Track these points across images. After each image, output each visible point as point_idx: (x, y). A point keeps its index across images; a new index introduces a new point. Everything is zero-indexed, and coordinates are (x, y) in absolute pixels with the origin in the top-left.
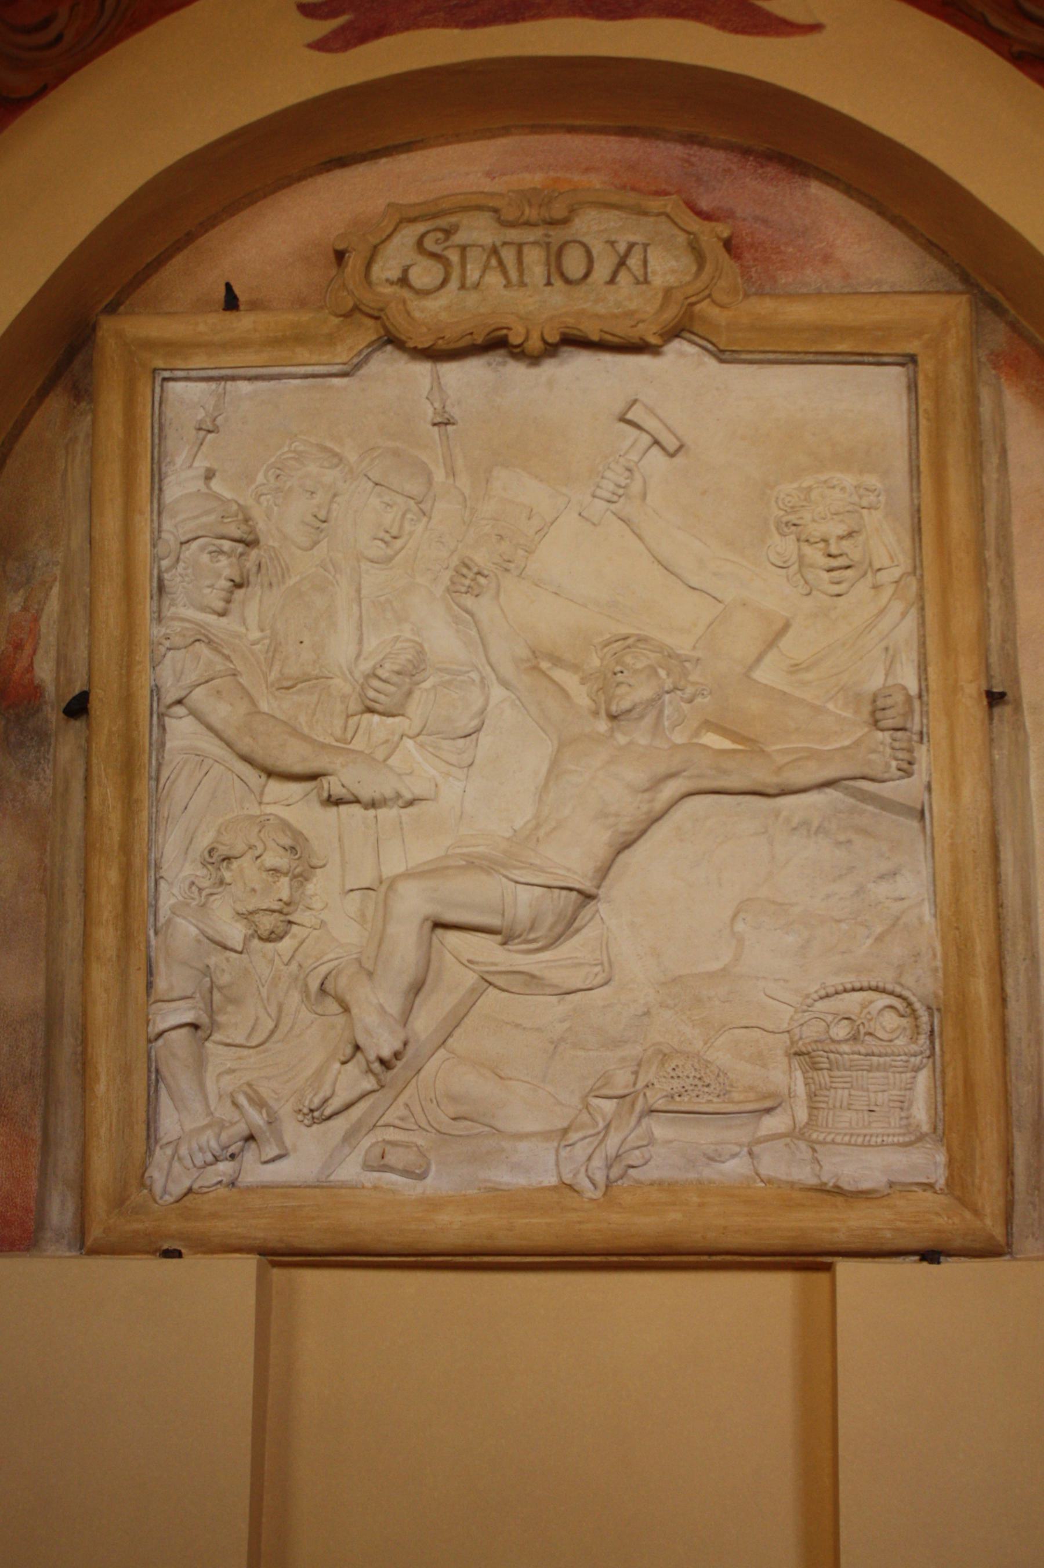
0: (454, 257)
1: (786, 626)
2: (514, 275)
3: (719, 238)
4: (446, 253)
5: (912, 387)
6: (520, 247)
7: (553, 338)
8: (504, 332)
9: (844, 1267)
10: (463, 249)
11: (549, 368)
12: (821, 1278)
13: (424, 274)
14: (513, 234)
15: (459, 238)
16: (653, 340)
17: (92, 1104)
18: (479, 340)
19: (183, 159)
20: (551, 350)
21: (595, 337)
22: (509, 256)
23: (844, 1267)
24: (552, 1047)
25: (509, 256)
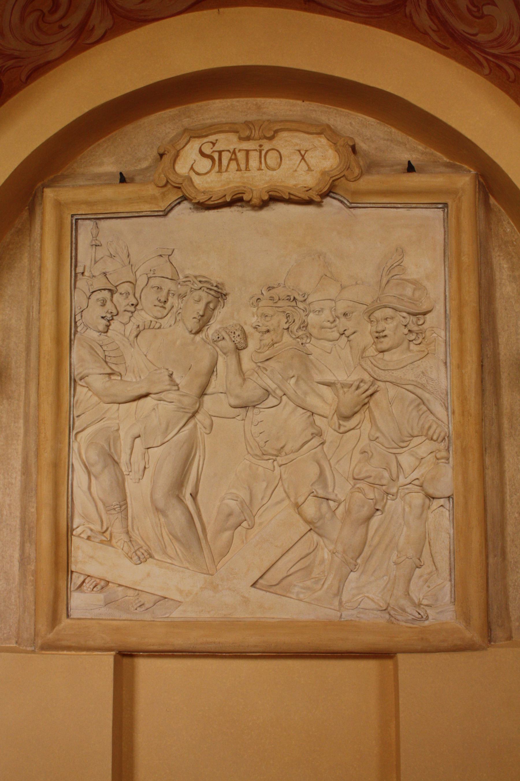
0: (216, 156)
1: (174, 250)
2: (243, 166)
3: (349, 145)
4: (213, 154)
5: (446, 219)
6: (247, 152)
7: (266, 198)
8: (241, 195)
9: (400, 656)
10: (220, 153)
11: (265, 214)
12: (389, 663)
13: (204, 165)
14: (246, 145)
15: (217, 147)
16: (317, 199)
17: (10, 367)
18: (228, 199)
19: (33, 152)
20: (264, 204)
21: (286, 197)
22: (241, 156)
23: (400, 656)
24: (104, 322)
25: (241, 156)
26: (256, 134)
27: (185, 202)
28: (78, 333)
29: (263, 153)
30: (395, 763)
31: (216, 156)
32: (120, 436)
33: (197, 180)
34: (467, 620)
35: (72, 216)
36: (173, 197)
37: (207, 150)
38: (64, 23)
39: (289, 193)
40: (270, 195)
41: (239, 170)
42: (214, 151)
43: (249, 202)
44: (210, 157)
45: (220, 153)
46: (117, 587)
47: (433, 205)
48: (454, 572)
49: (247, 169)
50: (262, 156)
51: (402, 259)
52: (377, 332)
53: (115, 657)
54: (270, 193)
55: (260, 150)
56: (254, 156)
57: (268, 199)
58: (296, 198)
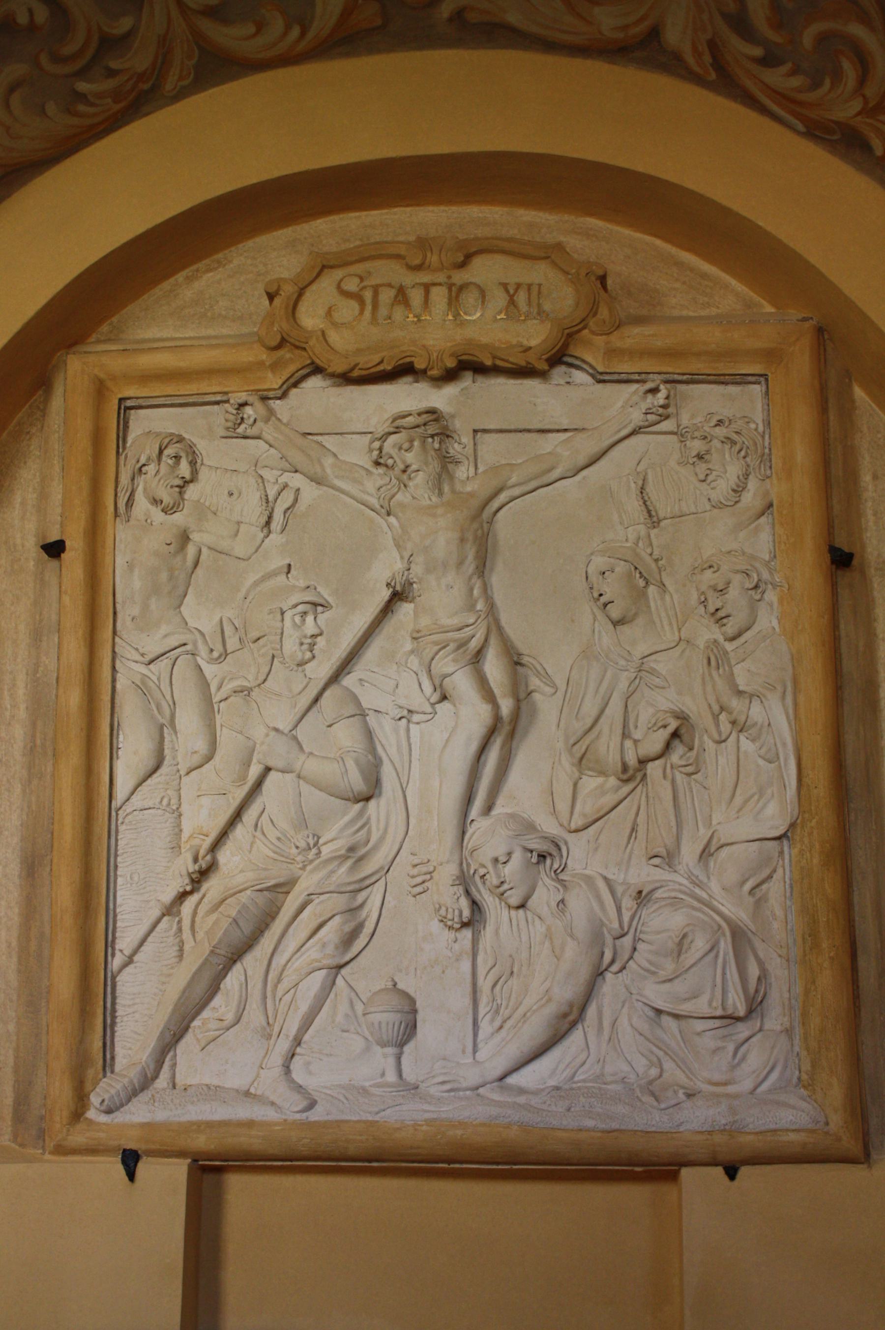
0: (368, 295)
7: (451, 363)
8: (408, 360)
12: (665, 1189)
16: (543, 366)
22: (416, 297)
23: (685, 1172)
26: (433, 259)
30: (762, 645)
31: (368, 295)
33: (334, 337)
35: (121, 400)
36: (294, 363)
37: (352, 285)
39: (494, 357)
40: (460, 362)
42: (364, 288)
43: (424, 372)
44: (358, 297)
45: (376, 290)
47: (123, 427)
52: (321, 1060)
53: (190, 1168)
54: (460, 358)
56: (439, 295)
57: (455, 367)
58: (510, 366)
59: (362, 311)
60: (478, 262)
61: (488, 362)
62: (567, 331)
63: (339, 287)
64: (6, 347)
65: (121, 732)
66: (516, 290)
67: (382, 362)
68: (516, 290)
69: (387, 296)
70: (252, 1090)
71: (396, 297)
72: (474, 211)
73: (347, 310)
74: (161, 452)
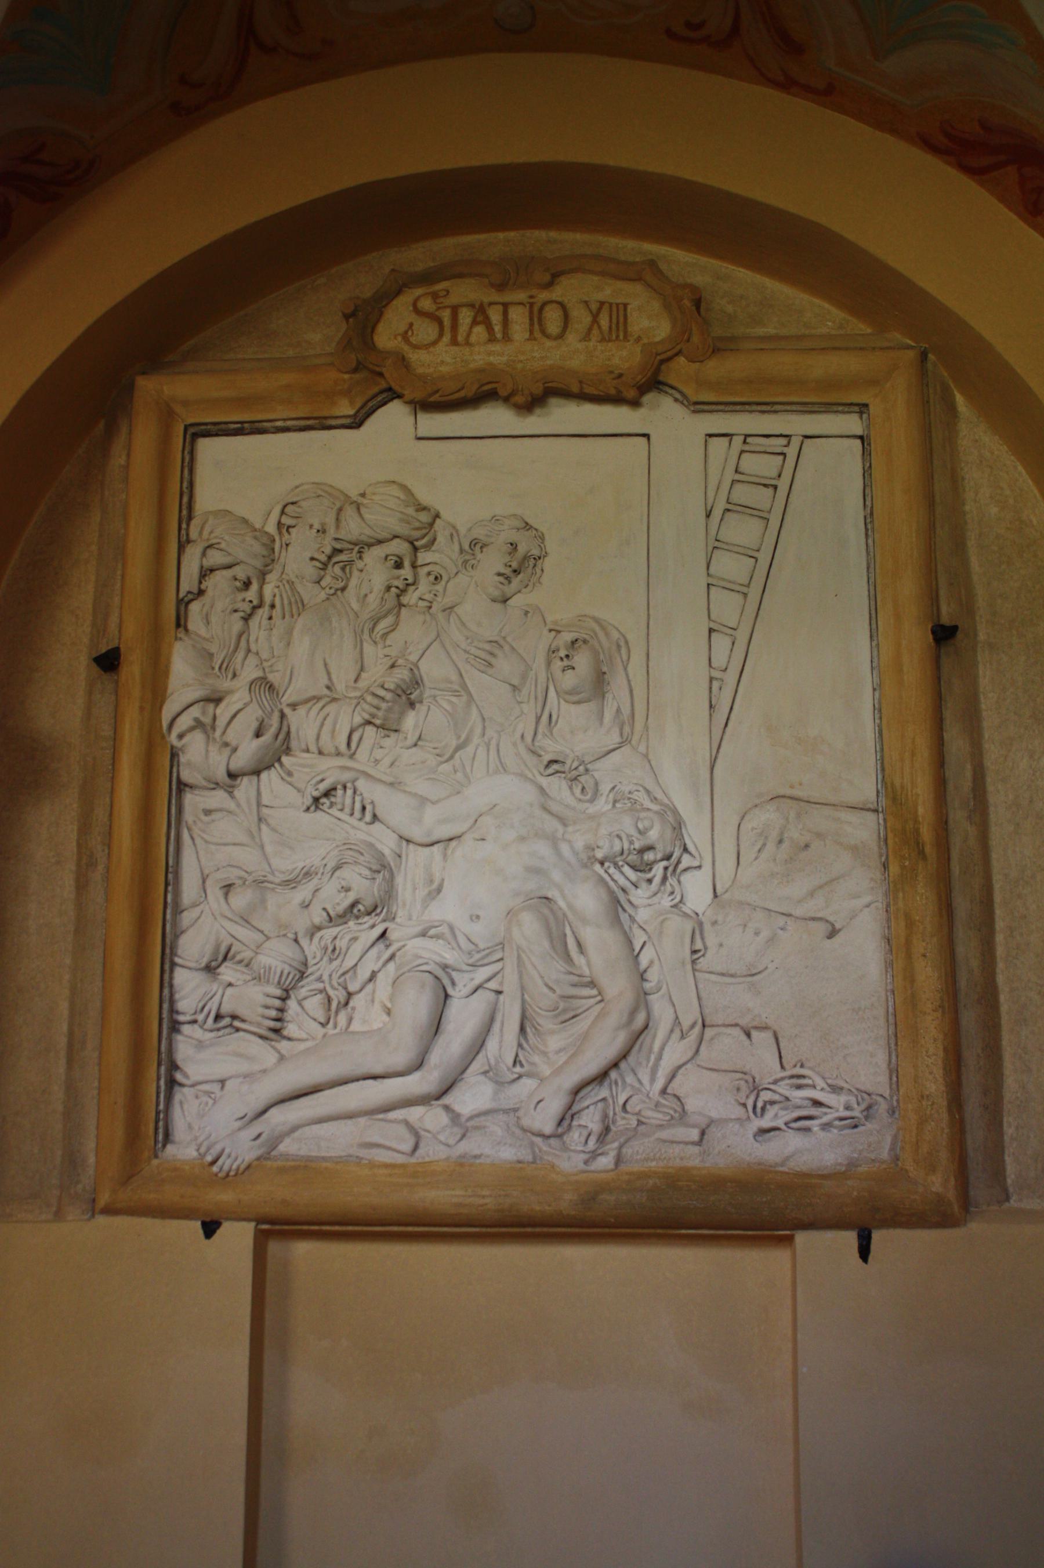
0: (446, 315)
22: (495, 316)
27: (396, 401)
28: (185, 423)
29: (536, 309)
31: (446, 315)
32: (383, 855)
34: (540, 747)
37: (426, 304)
38: (483, 998)
41: (492, 339)
45: (455, 310)
46: (415, 398)
48: (877, 637)
49: (507, 337)
50: (536, 317)
51: (358, 799)
54: (546, 385)
55: (529, 303)
56: (518, 316)
59: (441, 335)
60: (564, 281)
61: (575, 389)
62: (659, 358)
63: (415, 305)
64: (4, 424)
65: (185, 835)
66: (600, 309)
67: (463, 388)
68: (600, 309)
69: (466, 317)
70: (255, 778)
71: (475, 318)
72: (451, 241)
73: (426, 331)
74: (338, 868)
